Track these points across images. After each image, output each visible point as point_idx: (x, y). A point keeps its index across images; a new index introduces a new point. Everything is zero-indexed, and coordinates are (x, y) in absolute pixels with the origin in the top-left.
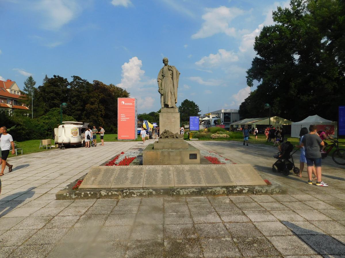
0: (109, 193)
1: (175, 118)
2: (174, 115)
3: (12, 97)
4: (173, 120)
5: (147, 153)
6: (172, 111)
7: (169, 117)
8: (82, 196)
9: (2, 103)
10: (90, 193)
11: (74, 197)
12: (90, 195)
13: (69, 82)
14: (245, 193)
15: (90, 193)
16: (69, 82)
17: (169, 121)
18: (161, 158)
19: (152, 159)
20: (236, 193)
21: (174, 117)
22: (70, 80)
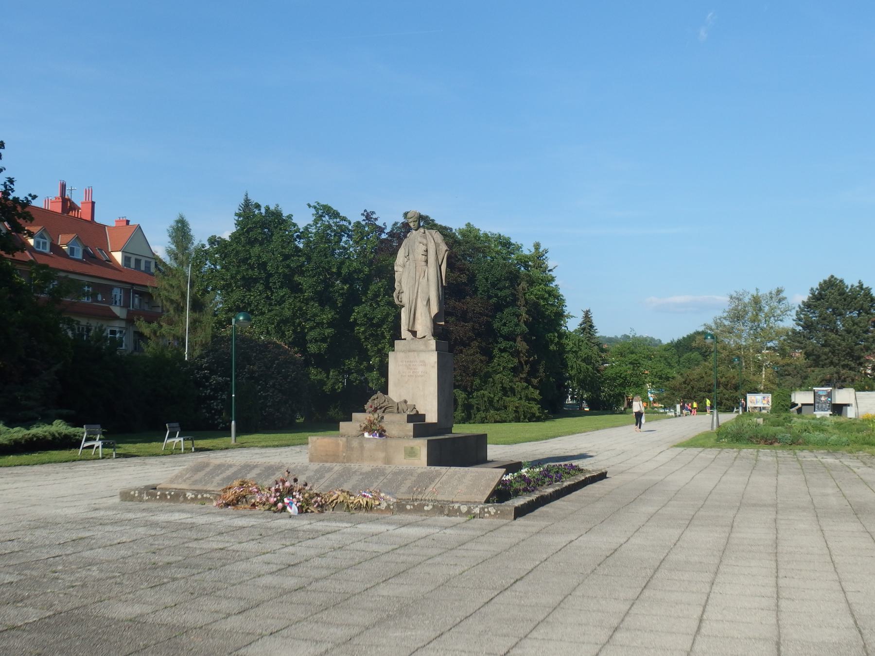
0: (197, 495)
1: (424, 363)
2: (424, 356)
3: (128, 281)
4: (420, 369)
5: (318, 441)
6: (422, 347)
7: (410, 362)
8: (158, 497)
9: (98, 301)
10: (170, 494)
11: (146, 498)
12: (169, 497)
13: (301, 225)
14: (428, 511)
15: (170, 494)
16: (301, 225)
17: (411, 374)
18: (344, 454)
19: (327, 455)
20: (219, 430)
21: (424, 361)
22: (303, 219)
